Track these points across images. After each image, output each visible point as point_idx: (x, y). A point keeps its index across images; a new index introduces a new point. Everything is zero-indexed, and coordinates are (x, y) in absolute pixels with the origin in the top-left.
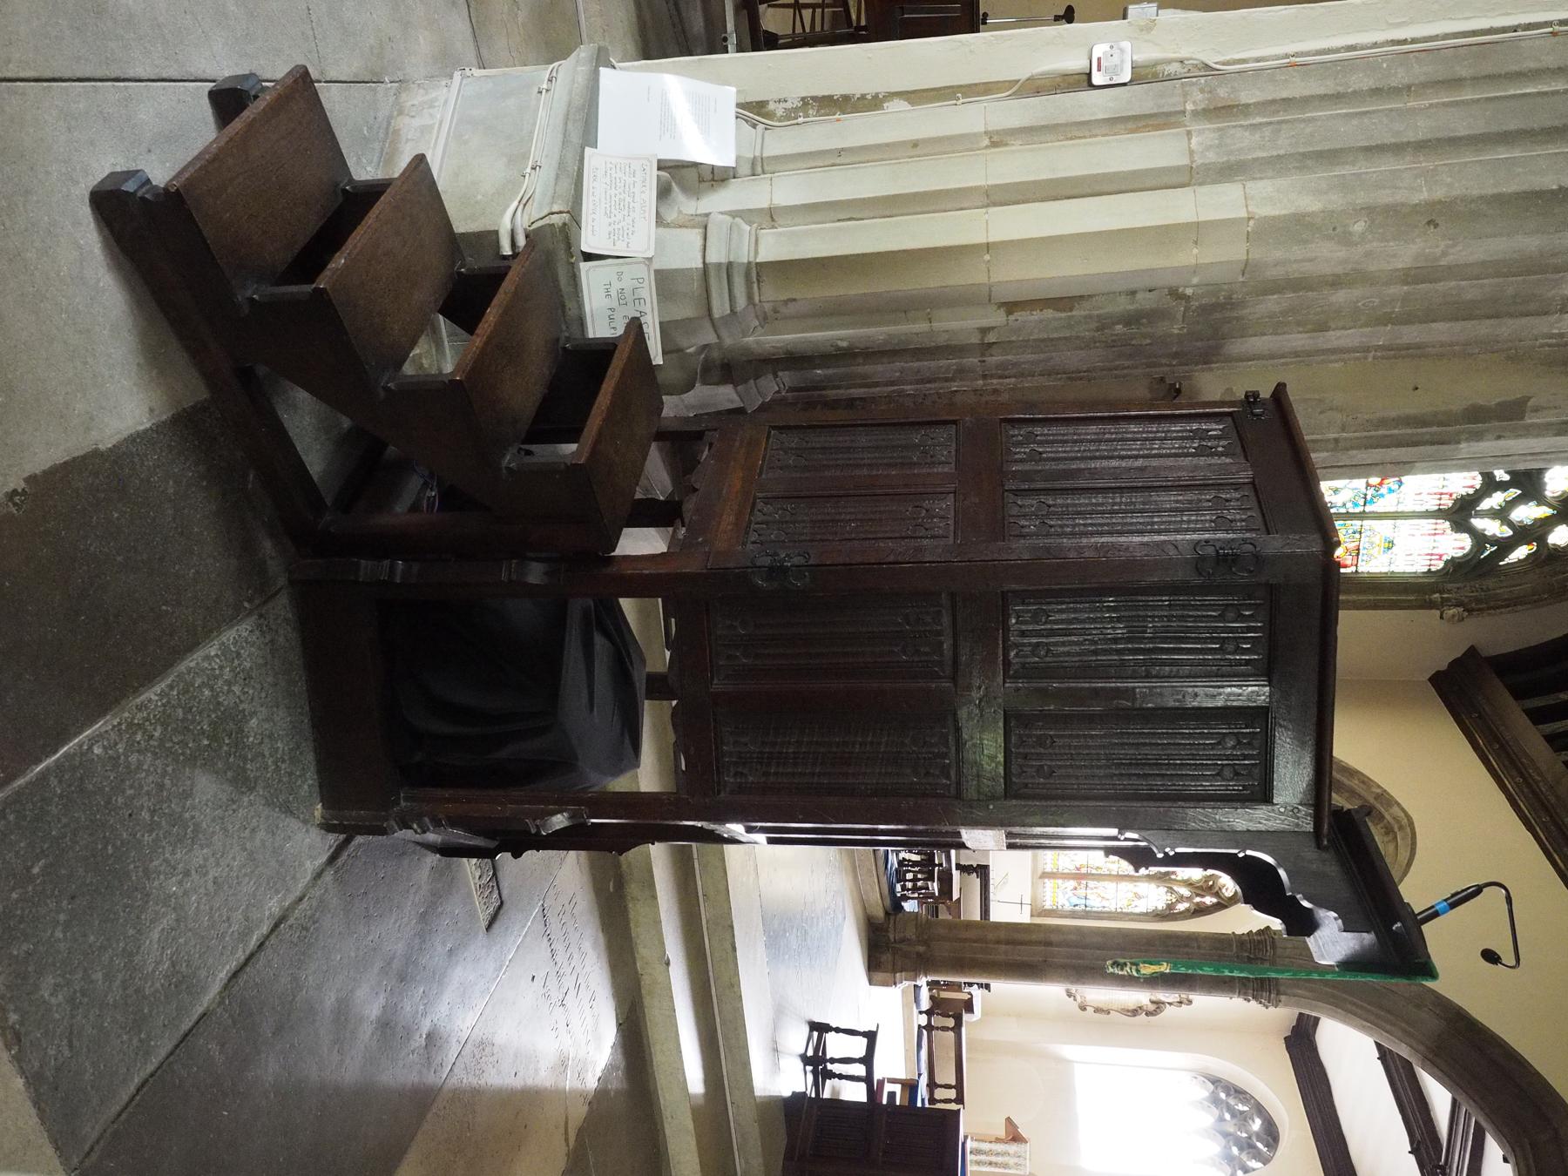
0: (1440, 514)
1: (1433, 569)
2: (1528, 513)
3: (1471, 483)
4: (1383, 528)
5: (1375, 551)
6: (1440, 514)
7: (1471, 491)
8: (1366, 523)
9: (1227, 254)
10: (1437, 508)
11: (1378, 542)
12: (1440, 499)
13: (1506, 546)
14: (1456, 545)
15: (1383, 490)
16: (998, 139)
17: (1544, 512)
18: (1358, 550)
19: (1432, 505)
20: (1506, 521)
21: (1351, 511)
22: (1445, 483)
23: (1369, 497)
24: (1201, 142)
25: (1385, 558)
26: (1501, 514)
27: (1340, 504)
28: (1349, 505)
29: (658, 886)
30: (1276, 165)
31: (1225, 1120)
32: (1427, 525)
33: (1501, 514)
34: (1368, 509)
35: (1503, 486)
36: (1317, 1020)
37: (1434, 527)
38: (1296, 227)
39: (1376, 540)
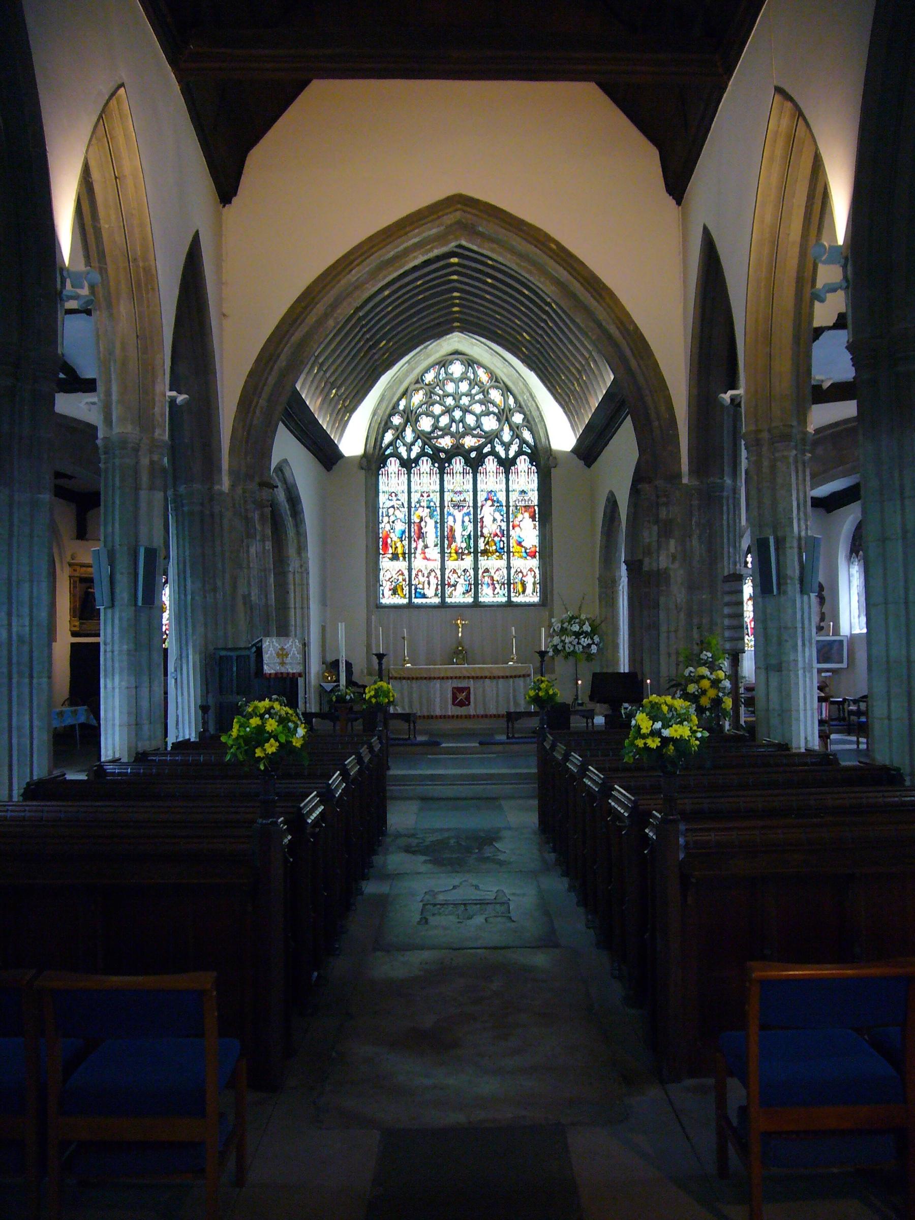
0: (507, 473)
1: (535, 471)
2: (506, 436)
3: (491, 461)
4: (513, 497)
5: (526, 498)
6: (507, 473)
7: (496, 460)
8: (511, 504)
9: (197, 657)
10: (504, 474)
11: (522, 498)
12: (499, 473)
13: (523, 442)
14: (523, 463)
15: (495, 499)
16: (182, 694)
17: (506, 428)
18: (526, 506)
19: (502, 477)
20: (511, 443)
21: (505, 512)
22: (491, 472)
23: (498, 505)
24: (184, 661)
25: (530, 494)
26: (507, 446)
27: (502, 518)
28: (464, 533)
29: (194, 719)
30: (187, 650)
31: (748, 567)
32: (512, 477)
33: (507, 446)
34: (504, 504)
35: (493, 447)
36: (812, 498)
37: (514, 474)
38: (194, 646)
39: (520, 498)
